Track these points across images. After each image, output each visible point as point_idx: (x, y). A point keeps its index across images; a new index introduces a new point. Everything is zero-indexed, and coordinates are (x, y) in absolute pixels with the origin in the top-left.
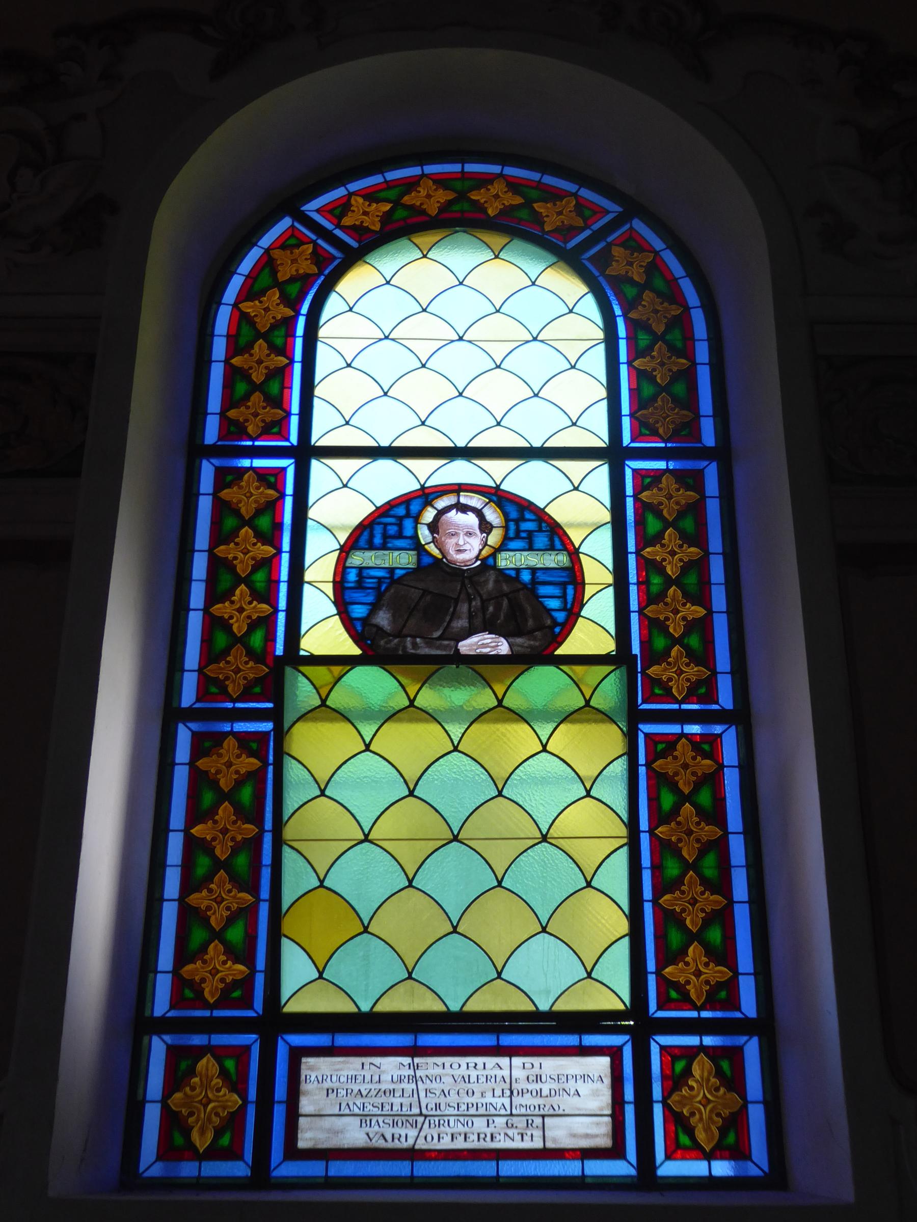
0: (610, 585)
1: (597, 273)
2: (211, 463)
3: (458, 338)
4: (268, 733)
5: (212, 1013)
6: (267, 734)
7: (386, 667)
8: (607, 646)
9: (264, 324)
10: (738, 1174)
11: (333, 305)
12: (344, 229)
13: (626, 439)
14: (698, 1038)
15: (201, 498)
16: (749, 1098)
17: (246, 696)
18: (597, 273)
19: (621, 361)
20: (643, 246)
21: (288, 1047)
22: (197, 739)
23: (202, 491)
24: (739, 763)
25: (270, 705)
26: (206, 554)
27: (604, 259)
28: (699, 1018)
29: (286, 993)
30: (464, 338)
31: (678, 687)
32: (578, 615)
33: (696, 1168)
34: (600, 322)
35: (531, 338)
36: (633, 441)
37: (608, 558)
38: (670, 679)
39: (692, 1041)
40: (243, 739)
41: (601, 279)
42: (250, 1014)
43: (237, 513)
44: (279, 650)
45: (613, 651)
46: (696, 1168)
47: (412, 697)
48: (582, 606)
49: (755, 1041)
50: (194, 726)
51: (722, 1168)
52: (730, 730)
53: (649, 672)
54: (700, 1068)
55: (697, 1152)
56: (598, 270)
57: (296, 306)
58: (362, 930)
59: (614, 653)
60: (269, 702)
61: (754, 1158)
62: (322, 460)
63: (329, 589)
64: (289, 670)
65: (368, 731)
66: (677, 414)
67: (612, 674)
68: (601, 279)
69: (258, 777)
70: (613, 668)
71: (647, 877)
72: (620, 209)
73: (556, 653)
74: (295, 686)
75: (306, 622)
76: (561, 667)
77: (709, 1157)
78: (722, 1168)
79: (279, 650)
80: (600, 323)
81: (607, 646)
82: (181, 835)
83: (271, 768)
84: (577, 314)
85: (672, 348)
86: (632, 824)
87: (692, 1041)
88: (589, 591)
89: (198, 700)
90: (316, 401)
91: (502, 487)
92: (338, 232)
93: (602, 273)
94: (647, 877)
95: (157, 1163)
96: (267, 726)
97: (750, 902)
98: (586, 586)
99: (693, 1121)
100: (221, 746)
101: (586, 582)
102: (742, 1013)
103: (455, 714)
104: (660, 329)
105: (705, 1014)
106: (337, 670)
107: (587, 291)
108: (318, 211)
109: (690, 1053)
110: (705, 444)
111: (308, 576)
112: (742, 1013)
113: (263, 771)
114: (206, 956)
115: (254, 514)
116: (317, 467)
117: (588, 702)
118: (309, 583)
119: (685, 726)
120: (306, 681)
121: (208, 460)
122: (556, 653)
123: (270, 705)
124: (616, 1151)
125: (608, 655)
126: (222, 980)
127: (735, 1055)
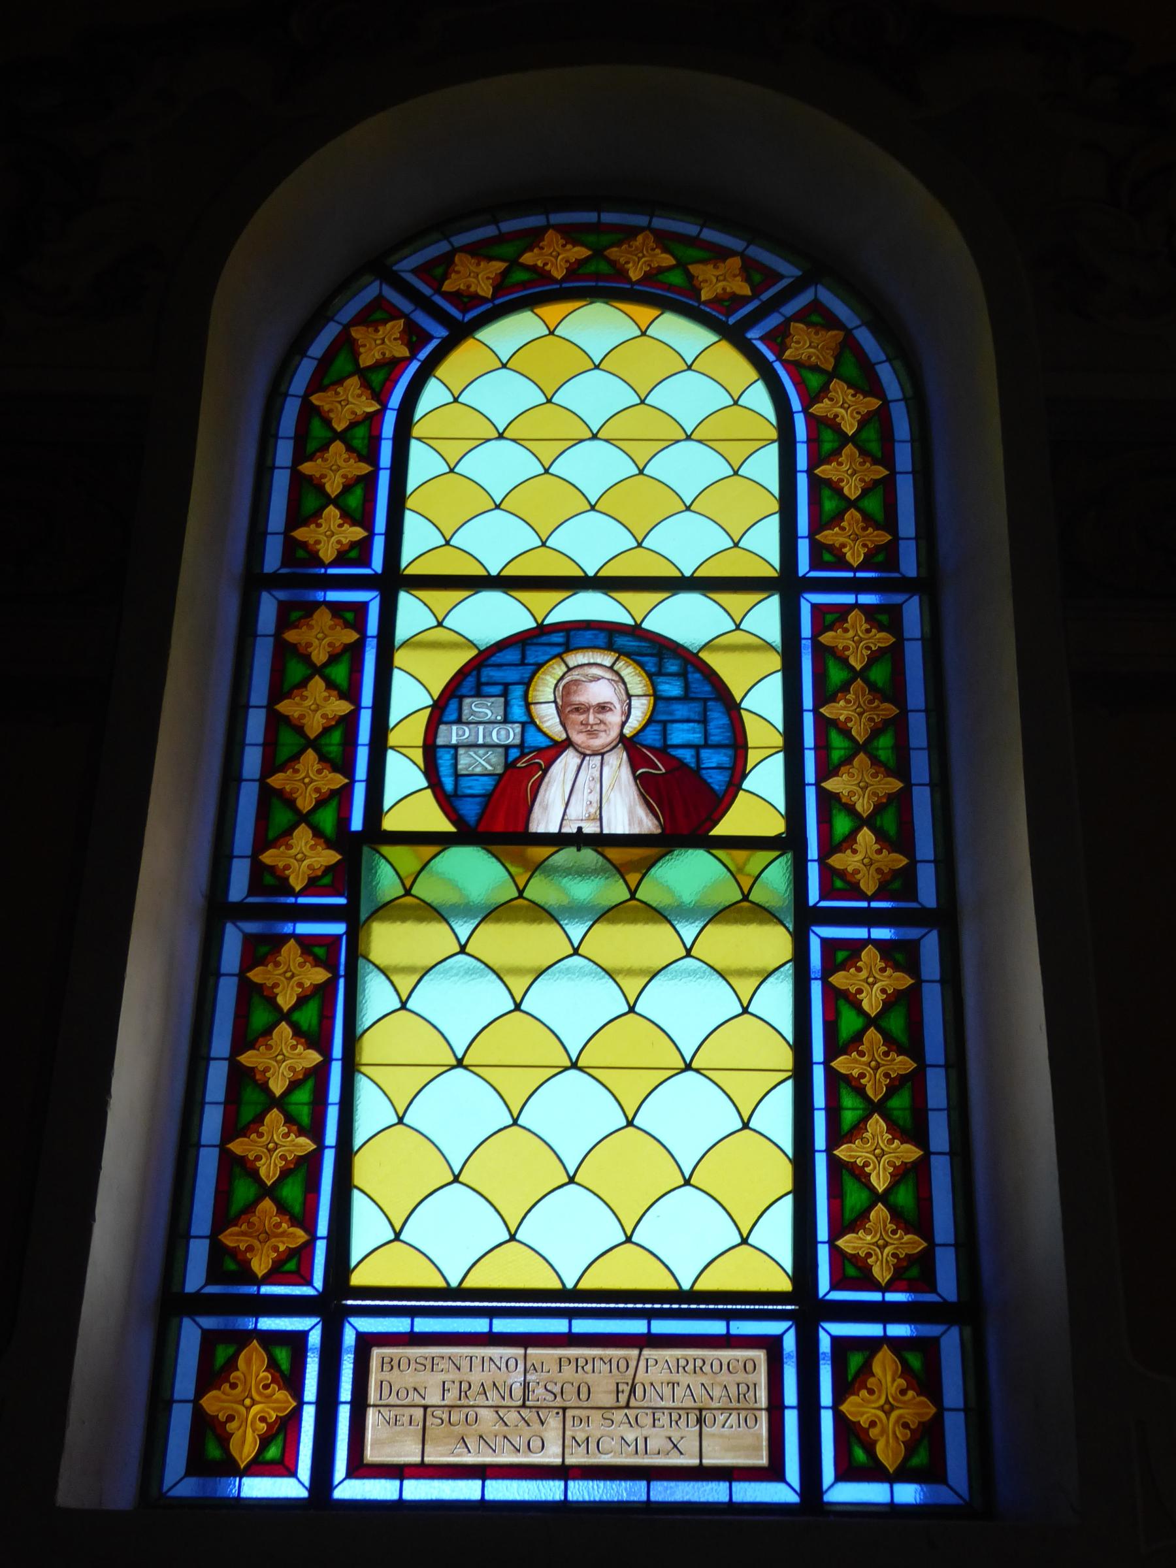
0: (773, 441)
1: (771, 357)
2: (273, 596)
3: (591, 436)
4: (339, 937)
5: (296, 900)
6: (338, 937)
7: (490, 848)
8: (775, 826)
9: (314, 725)
10: (929, 1501)
11: (433, 395)
12: (447, 296)
13: (803, 567)
14: (866, 930)
15: (269, 538)
16: (933, 1148)
17: (310, 889)
18: (771, 357)
19: (794, 410)
20: (831, 322)
21: (355, 1332)
22: (250, 942)
23: (252, 703)
24: (931, 780)
25: (342, 901)
26: (264, 711)
27: (778, 339)
28: (884, 1302)
29: (406, 558)
30: (599, 436)
31: (871, 999)
32: (739, 788)
33: (872, 1493)
34: (773, 418)
35: (684, 437)
36: (822, 898)
37: (776, 715)
38: (862, 1075)
39: (872, 1330)
40: (306, 943)
41: (778, 366)
42: (306, 1291)
43: (306, 659)
44: (357, 824)
45: (783, 833)
46: (872, 1493)
47: (521, 888)
48: (744, 776)
49: (954, 1332)
50: (282, 595)
51: (907, 1493)
52: (930, 935)
53: (840, 1243)
54: (884, 1365)
55: (873, 1472)
56: (774, 353)
57: (382, 397)
58: (451, 1178)
59: (784, 836)
60: (340, 895)
61: (951, 1482)
62: (413, 592)
63: (418, 755)
64: (366, 850)
65: (463, 930)
66: (890, 977)
67: (777, 862)
68: (778, 366)
69: (326, 992)
70: (777, 853)
71: (820, 1119)
72: (799, 273)
73: (712, 833)
74: (373, 870)
75: (390, 797)
76: (714, 852)
77: (891, 1479)
78: (907, 1493)
79: (357, 824)
80: (773, 420)
81: (775, 826)
82: (247, 862)
83: (342, 982)
84: (745, 407)
85: (868, 519)
86: (801, 1045)
87: (872, 1330)
88: (753, 757)
89: (283, 565)
90: (408, 514)
91: (644, 625)
92: (438, 299)
93: (779, 358)
94: (820, 1119)
95: (186, 1480)
96: (338, 928)
97: (951, 1153)
98: (750, 751)
99: (873, 1433)
100: (279, 952)
101: (749, 745)
102: (939, 1295)
103: (576, 911)
104: (880, 1183)
105: (891, 1297)
106: (428, 851)
107: (756, 378)
108: (415, 271)
109: (870, 1345)
110: (904, 572)
111: (416, 431)
112: (939, 1295)
113: (330, 986)
114: (262, 1128)
115: (315, 805)
116: (406, 601)
117: (745, 898)
118: (419, 439)
119: (859, 596)
120: (388, 867)
121: (234, 924)
122: (712, 833)
123: (342, 901)
124: (774, 1472)
125: (778, 837)
126: (283, 1157)
127: (927, 1347)
